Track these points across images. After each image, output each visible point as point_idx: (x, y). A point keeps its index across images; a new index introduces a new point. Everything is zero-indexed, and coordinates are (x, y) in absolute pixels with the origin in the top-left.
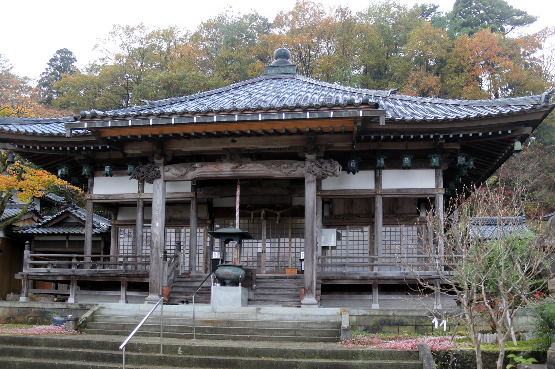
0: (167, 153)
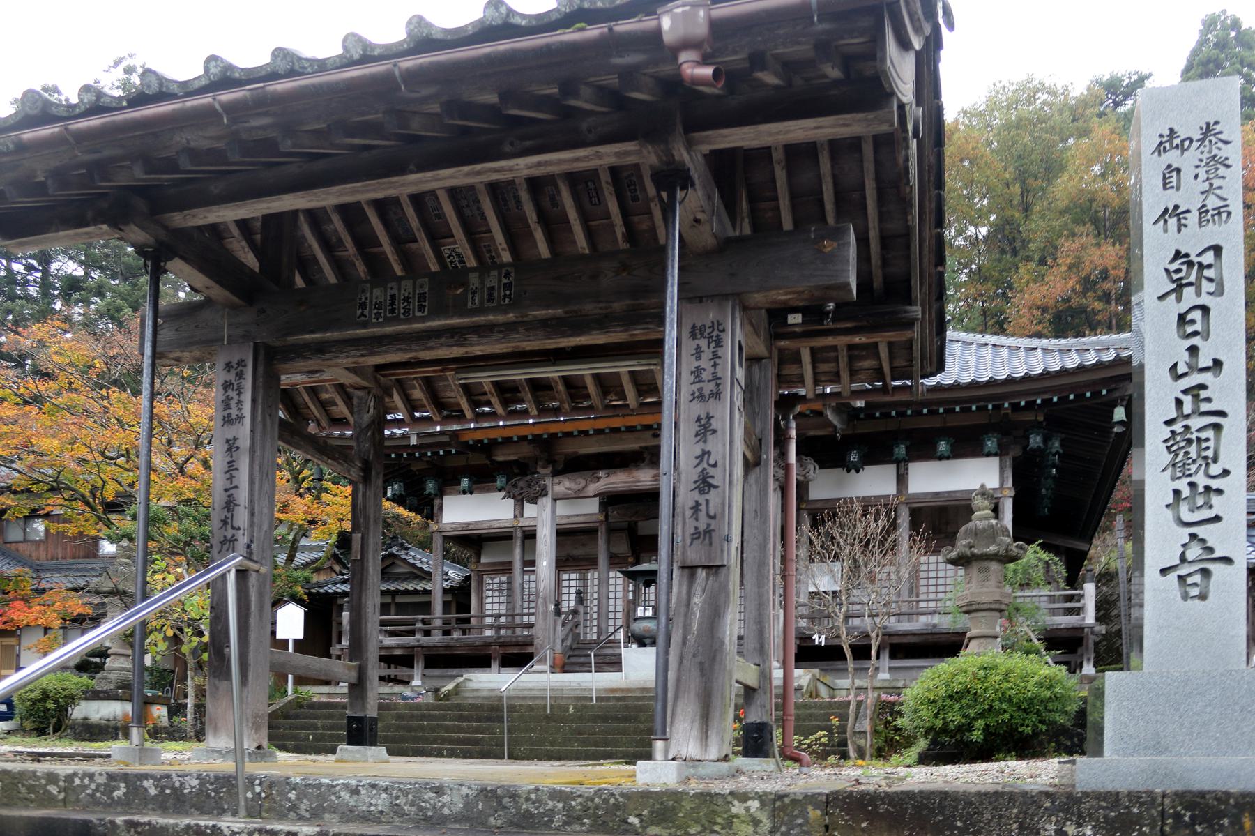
0: (557, 458)
